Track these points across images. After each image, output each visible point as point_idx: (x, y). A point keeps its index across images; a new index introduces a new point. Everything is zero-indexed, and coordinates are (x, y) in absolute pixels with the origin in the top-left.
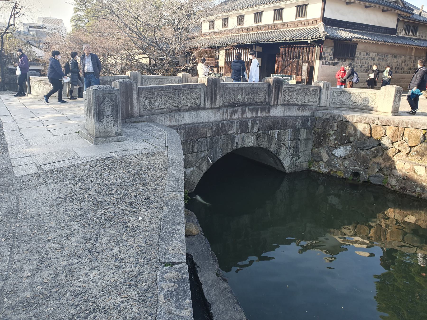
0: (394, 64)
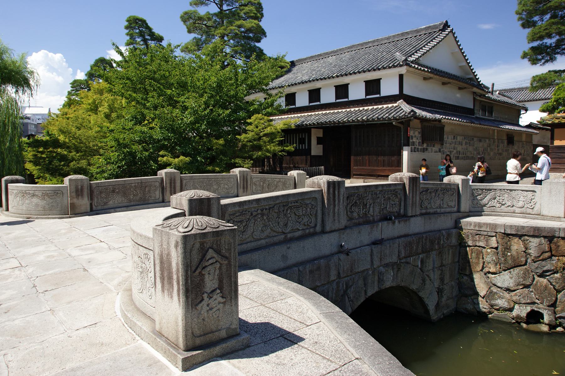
0: (480, 149)
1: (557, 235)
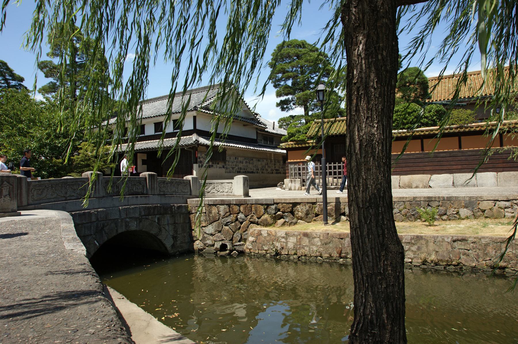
0: (259, 166)
1: (232, 203)
